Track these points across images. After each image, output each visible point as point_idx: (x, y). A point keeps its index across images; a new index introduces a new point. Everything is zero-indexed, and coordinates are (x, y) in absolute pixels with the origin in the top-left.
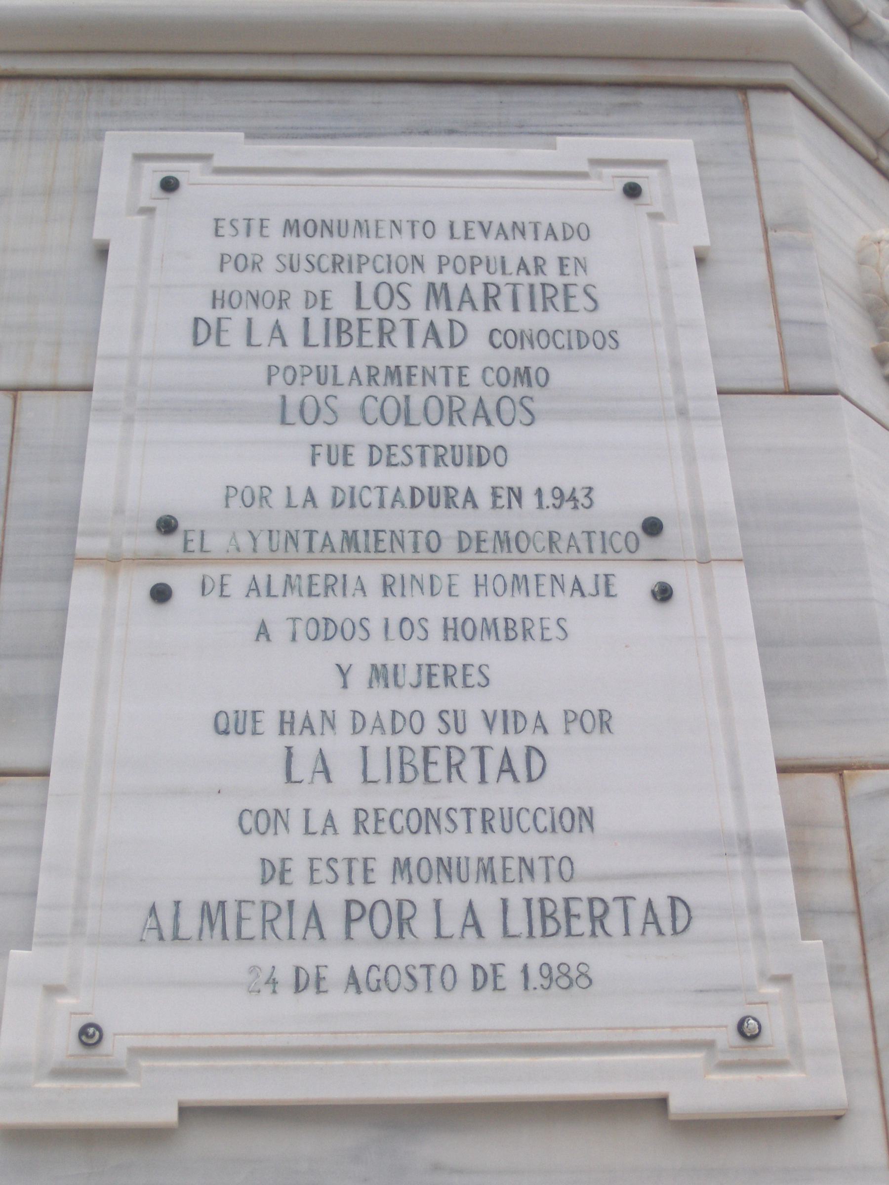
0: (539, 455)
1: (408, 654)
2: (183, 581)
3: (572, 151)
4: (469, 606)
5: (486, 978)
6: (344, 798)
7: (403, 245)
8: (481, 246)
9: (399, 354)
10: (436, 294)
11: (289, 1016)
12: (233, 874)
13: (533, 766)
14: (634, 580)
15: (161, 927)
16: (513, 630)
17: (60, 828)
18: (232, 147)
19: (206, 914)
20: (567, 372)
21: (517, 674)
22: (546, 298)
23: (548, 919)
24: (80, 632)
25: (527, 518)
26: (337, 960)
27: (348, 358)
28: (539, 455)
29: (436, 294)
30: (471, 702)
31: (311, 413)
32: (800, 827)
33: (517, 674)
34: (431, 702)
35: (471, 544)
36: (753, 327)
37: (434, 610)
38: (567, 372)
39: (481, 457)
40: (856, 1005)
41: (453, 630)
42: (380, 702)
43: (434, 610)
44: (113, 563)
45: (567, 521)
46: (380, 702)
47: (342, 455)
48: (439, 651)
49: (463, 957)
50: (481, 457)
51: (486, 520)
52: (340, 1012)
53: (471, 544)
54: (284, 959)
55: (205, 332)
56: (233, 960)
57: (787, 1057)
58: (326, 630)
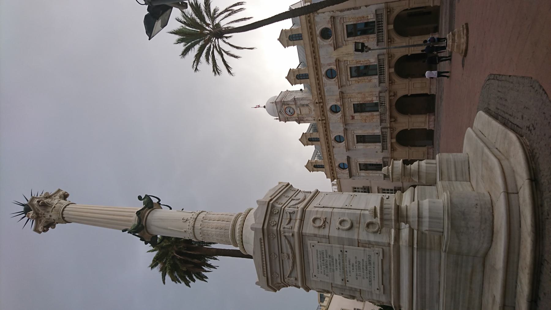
0: (336, 257)
1: (351, 268)
2: (347, 280)
3: (309, 249)
4: (348, 263)
5: (374, 267)
6: (362, 273)
7: (319, 262)
8: (319, 257)
9: (328, 264)
10: (323, 261)
11: (376, 278)
12: (367, 280)
13: (359, 263)
14: (345, 253)
15: (371, 285)
16: (349, 261)
17: (364, 289)
18: (311, 271)
19: (210, 58)
20: (329, 253)
21: (353, 261)
22: (323, 253)
23: (370, 264)
24: (351, 286)
25: (341, 258)
26: (373, 275)
27: (329, 267)
28: (336, 257)
29: (323, 261)
30: (355, 265)
31: (333, 270)
32: (363, 246)
33: (353, 261)
34: (355, 267)
35: (343, 262)
36: (324, 240)
37: (348, 266)
38: (329, 253)
39: (336, 260)
40: (375, 246)
41: (350, 264)
42: (355, 270)
43: (348, 266)
44: (345, 283)
45: (341, 256)
46: (355, 270)
47: (337, 269)
48: (351, 266)
49: (372, 268)
50: (336, 260)
51: (341, 261)
52: (376, 276)
53: (343, 262)
54: (373, 278)
55: (327, 275)
56: (373, 281)
57: (252, 255)
58: (350, 272)
